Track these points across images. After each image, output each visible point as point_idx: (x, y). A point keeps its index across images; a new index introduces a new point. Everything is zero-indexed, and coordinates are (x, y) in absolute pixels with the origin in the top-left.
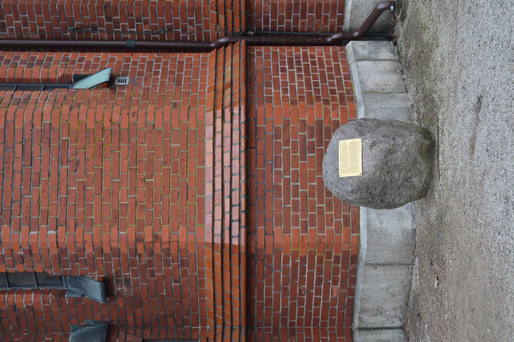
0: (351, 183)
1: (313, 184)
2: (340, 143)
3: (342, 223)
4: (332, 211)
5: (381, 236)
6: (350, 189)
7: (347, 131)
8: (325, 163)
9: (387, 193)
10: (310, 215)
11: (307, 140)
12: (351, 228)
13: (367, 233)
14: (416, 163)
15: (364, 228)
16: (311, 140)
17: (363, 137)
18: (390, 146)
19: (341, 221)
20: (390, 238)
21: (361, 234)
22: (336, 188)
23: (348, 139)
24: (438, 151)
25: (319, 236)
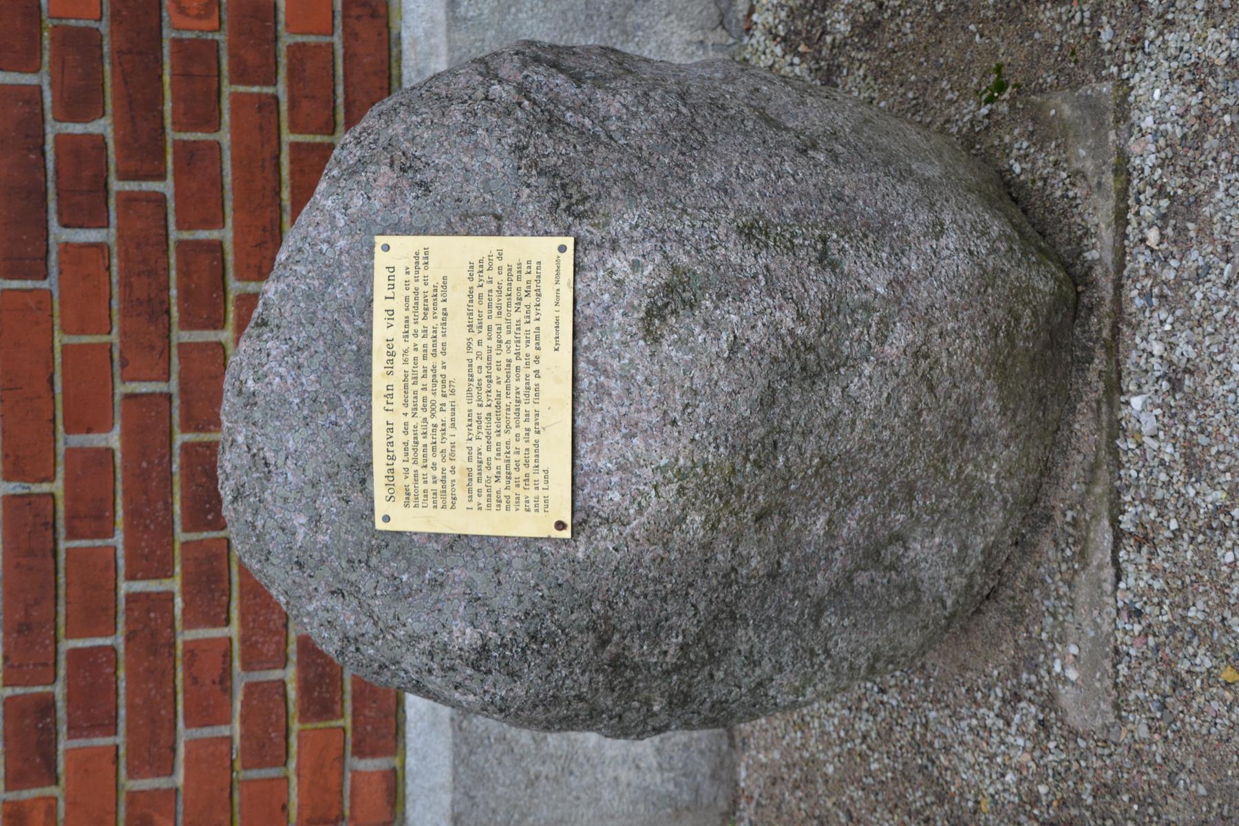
0: (470, 585)
1: (96, 440)
2: (381, 260)
3: (292, 694)
4: (227, 622)
5: (538, 767)
6: (465, 636)
7: (442, 160)
8: (250, 400)
9: (726, 651)
10: (74, 654)
11: (53, 128)
12: (347, 722)
13: (456, 754)
14: (964, 437)
15: (433, 725)
16: (78, 128)
17: (583, 228)
18: (801, 317)
19: (283, 684)
20: (588, 780)
21: (411, 762)
22: (331, 602)
23: (451, 231)
24: (1113, 347)
25: (133, 796)
